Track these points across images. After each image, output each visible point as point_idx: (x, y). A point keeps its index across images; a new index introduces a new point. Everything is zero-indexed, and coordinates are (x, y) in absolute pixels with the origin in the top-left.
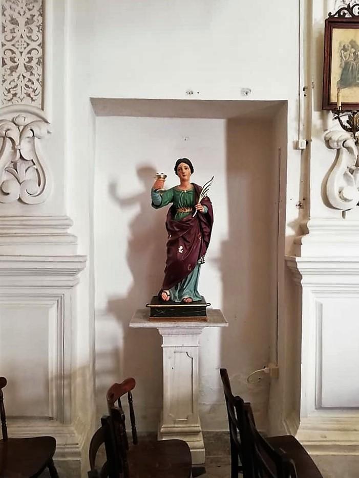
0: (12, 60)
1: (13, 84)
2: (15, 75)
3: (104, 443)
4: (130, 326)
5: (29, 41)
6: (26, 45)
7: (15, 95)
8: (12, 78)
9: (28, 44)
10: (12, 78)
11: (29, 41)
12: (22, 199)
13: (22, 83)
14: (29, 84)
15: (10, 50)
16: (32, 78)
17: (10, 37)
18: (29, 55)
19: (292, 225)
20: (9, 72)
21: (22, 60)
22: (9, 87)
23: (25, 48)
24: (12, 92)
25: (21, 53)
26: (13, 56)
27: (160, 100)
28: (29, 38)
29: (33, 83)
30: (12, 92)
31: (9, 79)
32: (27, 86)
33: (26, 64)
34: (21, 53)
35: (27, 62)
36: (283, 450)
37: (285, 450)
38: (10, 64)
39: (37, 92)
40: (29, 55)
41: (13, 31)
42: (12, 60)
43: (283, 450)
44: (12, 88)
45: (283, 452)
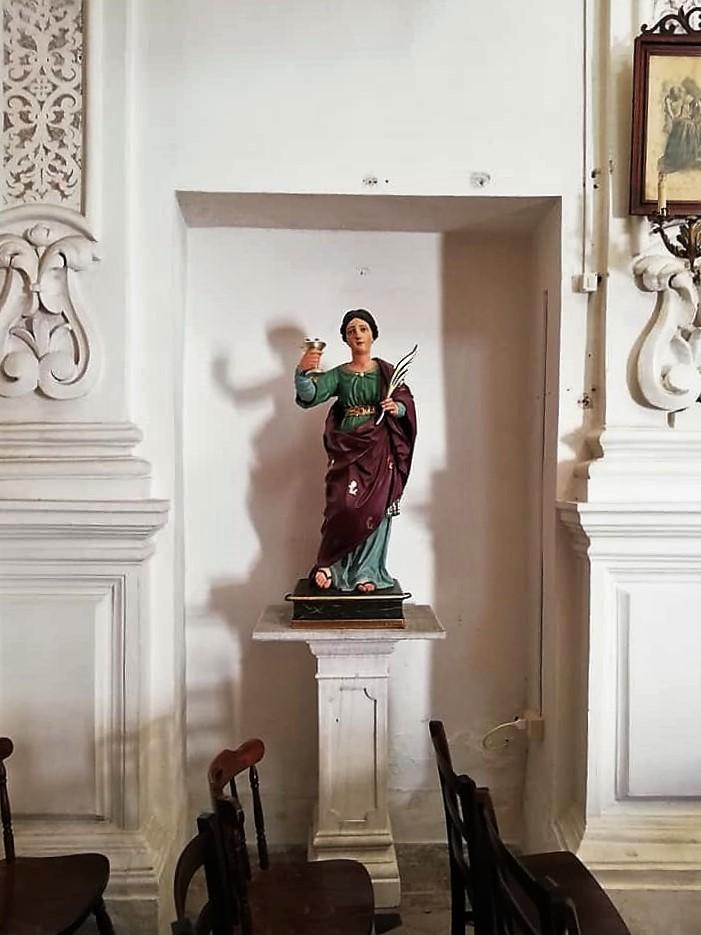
0: (24, 117)
1: (26, 165)
2: (29, 146)
3: (202, 867)
4: (254, 637)
5: (56, 81)
6: (50, 88)
7: (29, 186)
8: (23, 153)
9: (55, 87)
10: (23, 153)
11: (56, 81)
12: (44, 389)
13: (43, 162)
14: (57, 164)
15: (20, 97)
16: (63, 153)
17: (19, 73)
18: (57, 108)
19: (571, 441)
20: (17, 140)
21: (42, 118)
22: (17, 170)
23: (49, 94)
24: (24, 179)
25: (42, 103)
26: (25, 109)
27: (312, 195)
28: (57, 74)
29: (64, 163)
30: (24, 179)
31: (18, 154)
32: (53, 169)
33: (50, 124)
34: (42, 103)
35: (52, 122)
36: (552, 881)
37: (556, 881)
38: (19, 125)
39: (72, 180)
40: (57, 108)
41: (25, 60)
42: (24, 117)
43: (552, 881)
44: (23, 172)
45: (552, 885)
